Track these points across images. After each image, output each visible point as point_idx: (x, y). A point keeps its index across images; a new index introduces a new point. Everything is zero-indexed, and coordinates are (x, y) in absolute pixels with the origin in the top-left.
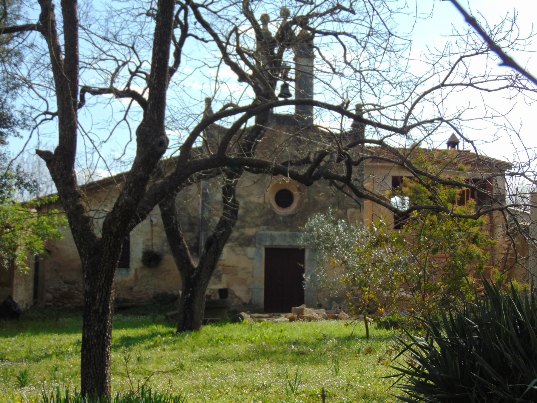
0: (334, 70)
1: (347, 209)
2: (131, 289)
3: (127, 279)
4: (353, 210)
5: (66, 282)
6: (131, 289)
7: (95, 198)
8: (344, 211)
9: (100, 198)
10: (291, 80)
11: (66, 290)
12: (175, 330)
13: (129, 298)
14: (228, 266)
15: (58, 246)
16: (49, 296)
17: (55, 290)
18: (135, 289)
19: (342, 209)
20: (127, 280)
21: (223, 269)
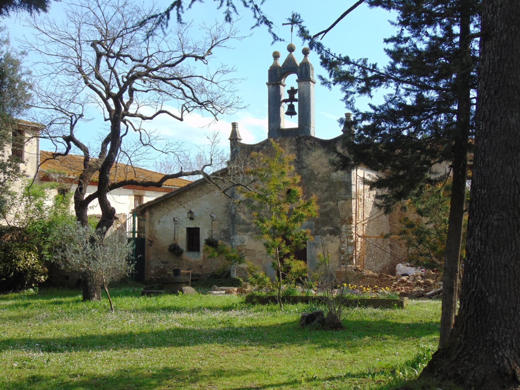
0: (39, 166)
1: (338, 201)
2: (201, 267)
3: (199, 260)
4: (343, 202)
5: (163, 263)
6: (201, 267)
7: (178, 202)
8: (336, 203)
9: (181, 202)
10: (296, 100)
11: (162, 268)
12: (80, 297)
13: (200, 273)
14: (249, 250)
15: (157, 237)
16: (153, 272)
17: (156, 267)
18: (204, 267)
19: (334, 202)
20: (199, 260)
21: (245, 252)
